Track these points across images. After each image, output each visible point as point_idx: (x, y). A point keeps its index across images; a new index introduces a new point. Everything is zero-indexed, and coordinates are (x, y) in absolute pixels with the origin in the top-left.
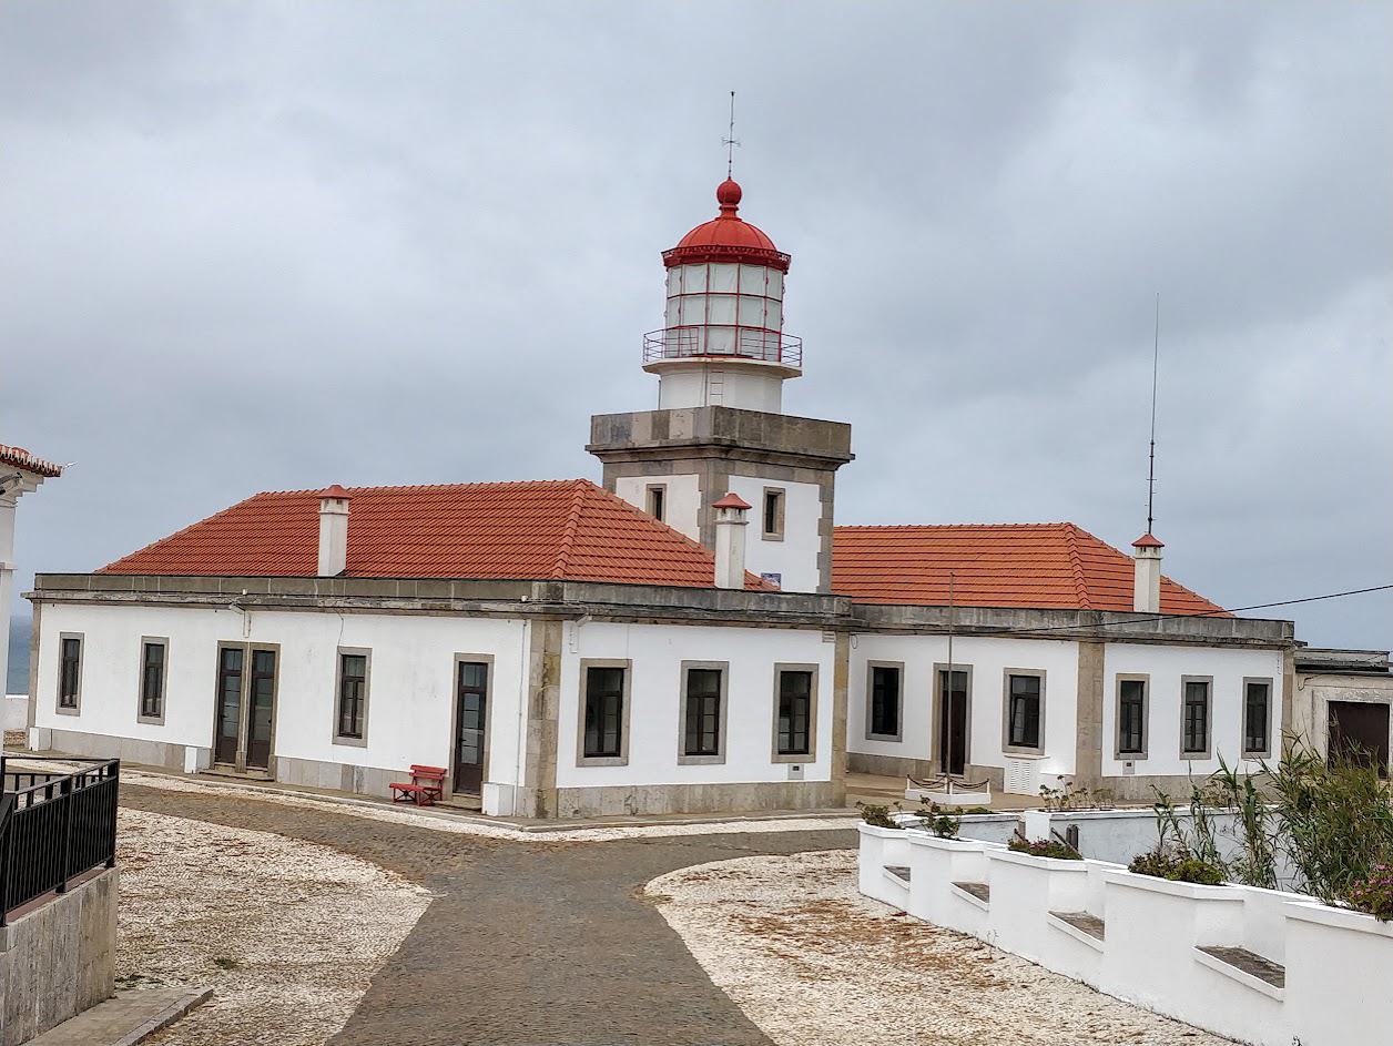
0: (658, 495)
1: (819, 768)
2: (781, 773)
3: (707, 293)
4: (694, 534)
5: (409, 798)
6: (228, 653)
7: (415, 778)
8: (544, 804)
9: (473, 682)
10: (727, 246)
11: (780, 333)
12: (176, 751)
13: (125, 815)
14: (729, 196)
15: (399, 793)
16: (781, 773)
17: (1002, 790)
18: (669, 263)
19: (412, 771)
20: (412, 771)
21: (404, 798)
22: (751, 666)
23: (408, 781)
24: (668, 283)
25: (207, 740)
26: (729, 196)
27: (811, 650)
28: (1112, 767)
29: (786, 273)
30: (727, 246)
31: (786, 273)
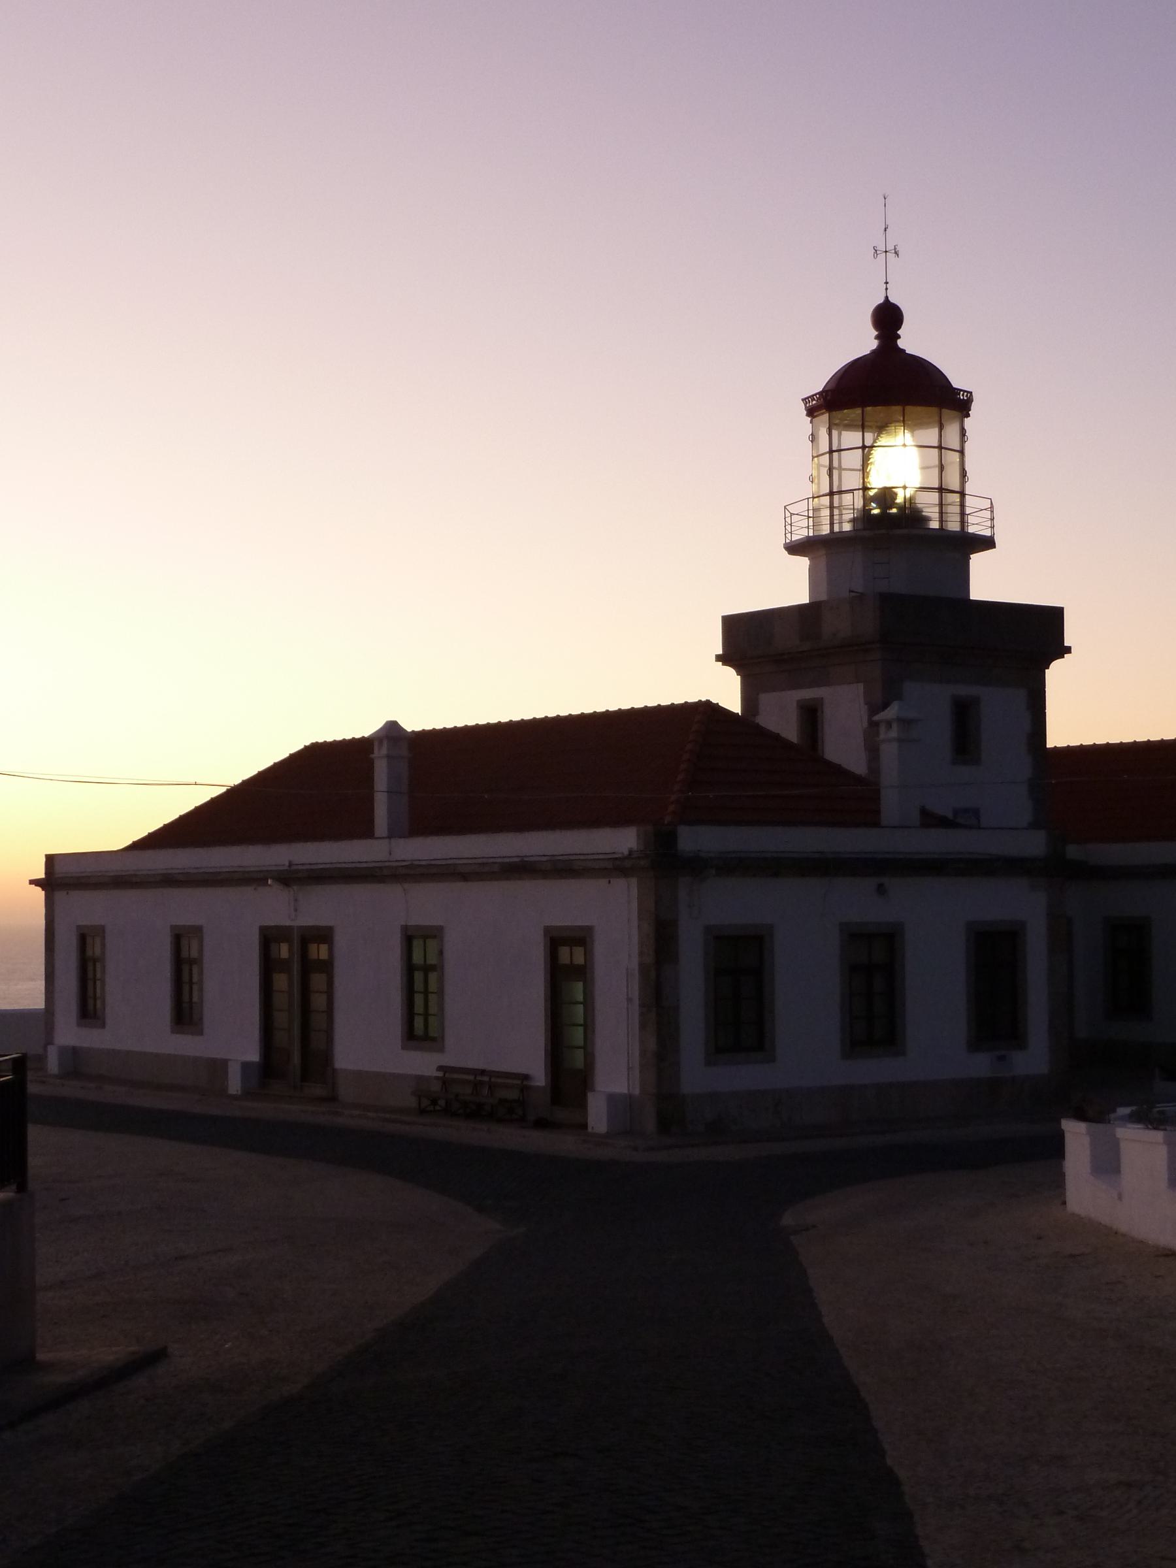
0: (811, 715)
1: (1034, 1059)
2: (980, 1065)
3: (940, 447)
4: (857, 764)
5: (438, 1108)
6: (269, 938)
7: (444, 1083)
8: (668, 1108)
9: (566, 962)
10: (887, 384)
11: (962, 494)
12: (218, 1067)
13: (35, 1134)
14: (888, 318)
15: (425, 1102)
16: (980, 1065)
17: (584, 1126)
18: (811, 412)
19: (440, 1074)
20: (440, 1074)
21: (431, 1108)
22: (935, 932)
23: (436, 1087)
24: (813, 438)
25: (254, 1056)
26: (888, 318)
27: (1024, 905)
28: (698, 1075)
29: (968, 416)
30: (887, 384)
31: (968, 416)
